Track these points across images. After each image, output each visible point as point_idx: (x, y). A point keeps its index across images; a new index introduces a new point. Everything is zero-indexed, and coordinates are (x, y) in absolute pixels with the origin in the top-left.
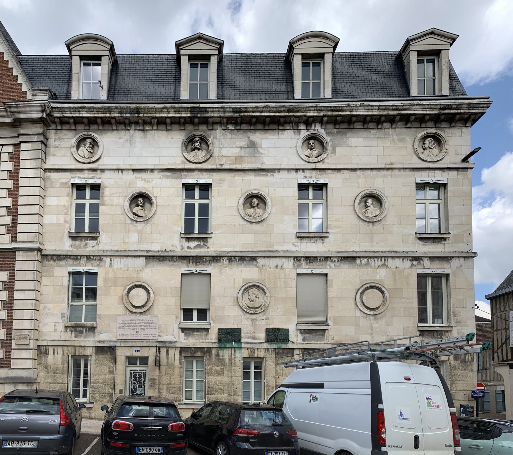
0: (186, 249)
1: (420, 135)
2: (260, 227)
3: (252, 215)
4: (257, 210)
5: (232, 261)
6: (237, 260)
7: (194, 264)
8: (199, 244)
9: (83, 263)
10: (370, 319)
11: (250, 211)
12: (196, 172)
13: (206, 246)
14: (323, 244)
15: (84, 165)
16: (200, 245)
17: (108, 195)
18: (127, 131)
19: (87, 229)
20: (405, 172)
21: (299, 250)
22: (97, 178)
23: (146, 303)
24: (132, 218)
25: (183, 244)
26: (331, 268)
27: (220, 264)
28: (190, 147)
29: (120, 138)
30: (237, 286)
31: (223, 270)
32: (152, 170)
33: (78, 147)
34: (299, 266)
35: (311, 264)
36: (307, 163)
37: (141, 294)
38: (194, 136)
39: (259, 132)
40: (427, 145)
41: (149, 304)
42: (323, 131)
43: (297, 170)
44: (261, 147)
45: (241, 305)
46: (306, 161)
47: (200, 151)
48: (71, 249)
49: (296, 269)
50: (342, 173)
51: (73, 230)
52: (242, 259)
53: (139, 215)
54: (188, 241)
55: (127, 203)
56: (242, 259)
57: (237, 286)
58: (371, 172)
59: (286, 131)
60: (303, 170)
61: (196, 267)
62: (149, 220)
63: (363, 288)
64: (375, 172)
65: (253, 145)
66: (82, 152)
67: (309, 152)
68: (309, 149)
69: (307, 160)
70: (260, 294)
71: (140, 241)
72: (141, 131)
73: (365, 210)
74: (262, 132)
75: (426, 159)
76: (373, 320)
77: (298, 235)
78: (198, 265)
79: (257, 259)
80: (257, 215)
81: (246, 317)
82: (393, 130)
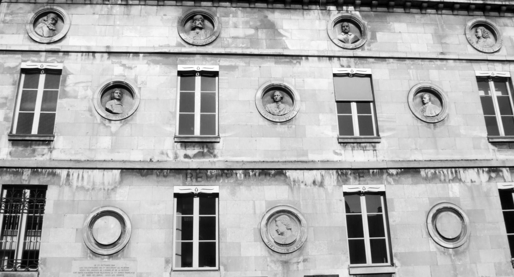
0: (181, 158)
1: (470, 24)
2: (286, 129)
3: (276, 113)
4: (282, 106)
5: (249, 176)
6: (257, 174)
7: (194, 180)
8: (201, 150)
9: (26, 179)
10: (450, 255)
11: (272, 107)
12: (198, 57)
13: (212, 153)
14: (375, 152)
15: (42, 45)
16: (203, 152)
17: (71, 85)
18: (104, 6)
19: (35, 130)
20: (461, 64)
21: (344, 160)
22: (58, 62)
23: (119, 238)
24: (104, 115)
25: (178, 152)
26: (389, 183)
27: (232, 180)
28: (189, 24)
29: (94, 14)
30: (258, 212)
31: (237, 188)
32: (136, 53)
33: (35, 22)
34: (346, 181)
35: (361, 179)
36: (342, 49)
37: (112, 226)
38: (195, 14)
39: (278, 11)
40: (480, 34)
41: (124, 241)
42: (358, 13)
43: (330, 57)
44: (282, 29)
45: (266, 240)
46: (341, 47)
47: (203, 31)
48: (9, 158)
49: (341, 186)
50: (387, 62)
51: (14, 132)
52: (264, 172)
53: (114, 111)
54: (185, 147)
55: (97, 95)
56: (264, 172)
57: (258, 212)
58: (423, 63)
59: (312, 12)
60: (339, 57)
61: (196, 184)
62: (129, 118)
63: (434, 211)
64: (427, 62)
65: (271, 27)
66: (40, 30)
67: (342, 36)
68: (343, 32)
69: (341, 46)
70: (293, 225)
71: (113, 149)
72: (123, 6)
73: (422, 107)
74: (282, 11)
75: (481, 50)
76: (454, 256)
77: (340, 140)
78: (200, 182)
79: (286, 173)
80: (282, 113)
81: (273, 259)
82: (440, 16)
